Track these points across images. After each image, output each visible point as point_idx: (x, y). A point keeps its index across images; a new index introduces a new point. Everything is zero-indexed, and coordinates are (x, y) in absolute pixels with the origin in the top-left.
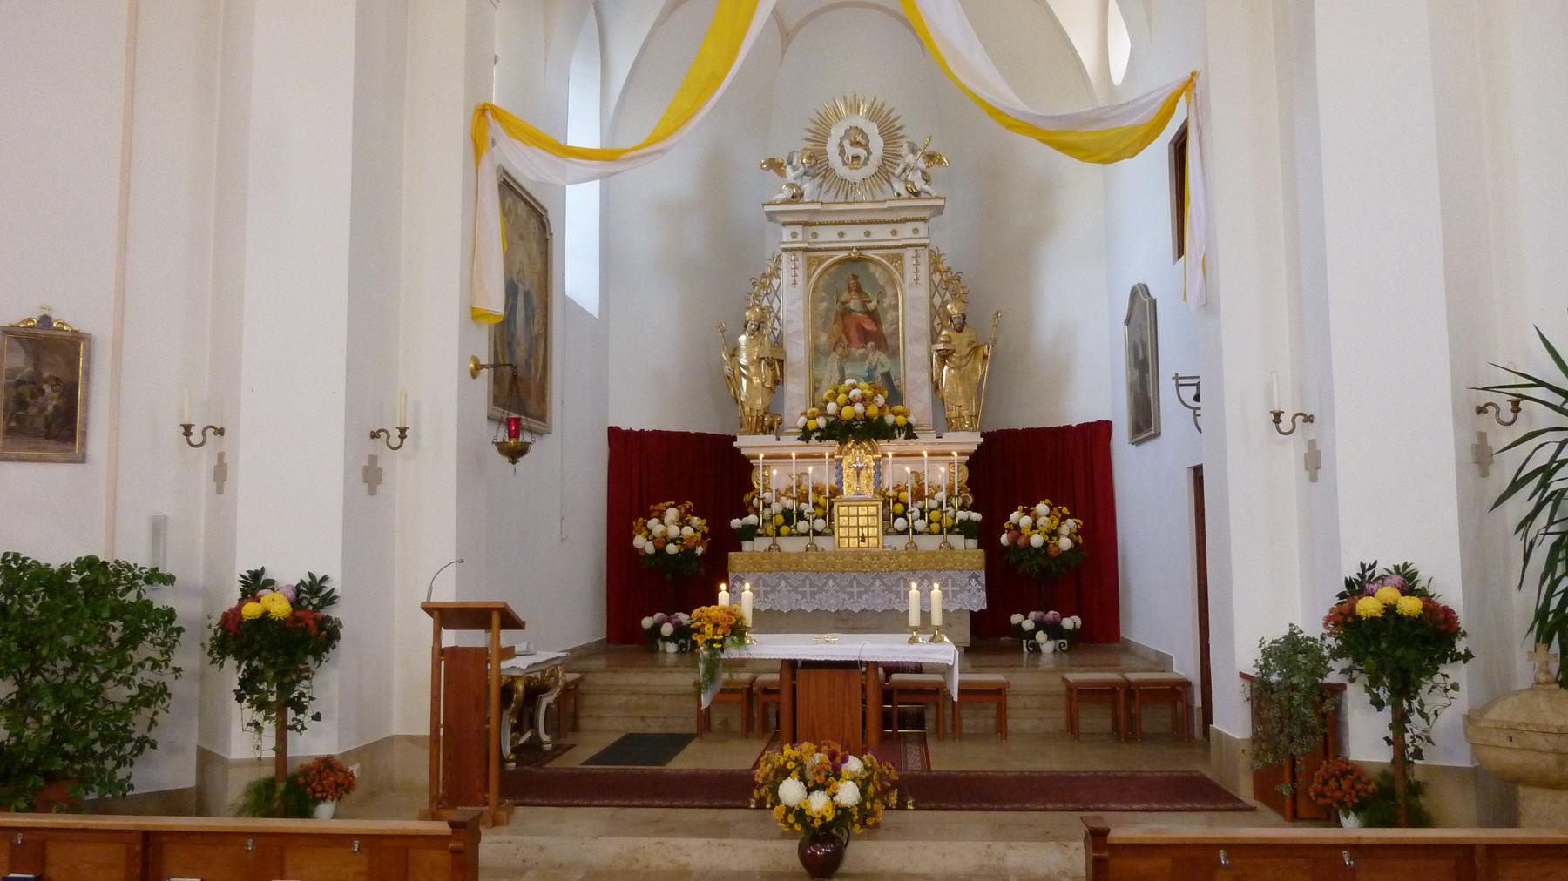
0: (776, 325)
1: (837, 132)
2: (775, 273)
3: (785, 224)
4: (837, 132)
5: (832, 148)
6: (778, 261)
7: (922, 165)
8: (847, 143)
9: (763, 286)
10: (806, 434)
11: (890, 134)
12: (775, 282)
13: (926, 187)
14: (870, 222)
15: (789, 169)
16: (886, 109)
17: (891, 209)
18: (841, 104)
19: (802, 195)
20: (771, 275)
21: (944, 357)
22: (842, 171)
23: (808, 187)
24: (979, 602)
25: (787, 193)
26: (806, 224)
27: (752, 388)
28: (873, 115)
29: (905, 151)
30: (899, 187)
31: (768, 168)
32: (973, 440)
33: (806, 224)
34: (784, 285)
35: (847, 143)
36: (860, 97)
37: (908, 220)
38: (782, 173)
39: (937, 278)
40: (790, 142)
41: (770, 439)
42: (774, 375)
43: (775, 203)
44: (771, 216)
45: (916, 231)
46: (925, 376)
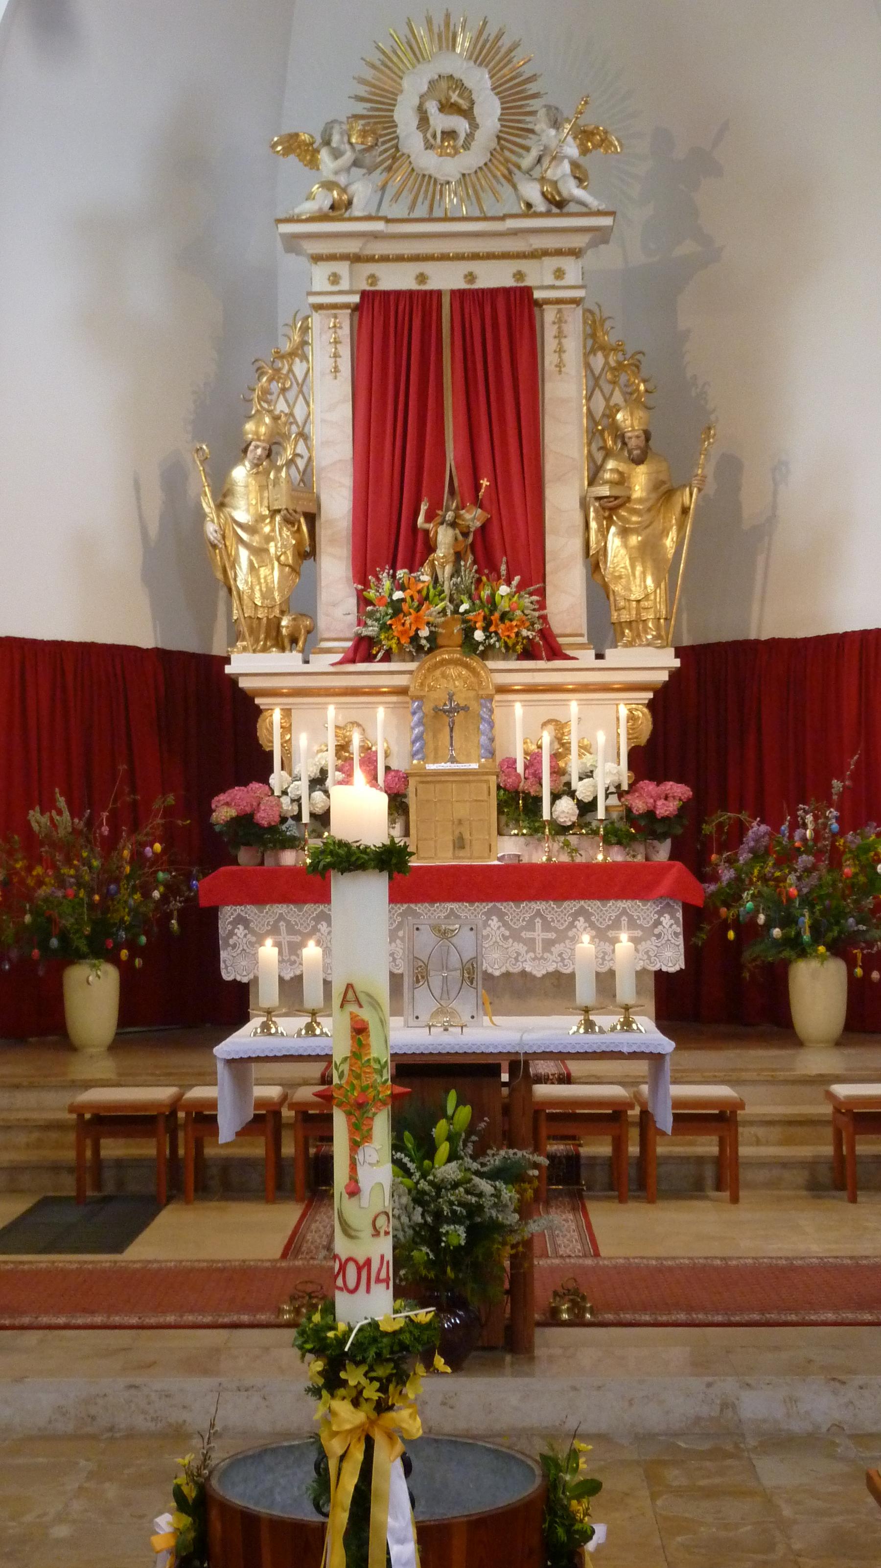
0: (301, 448)
1: (413, 86)
2: (300, 351)
3: (317, 258)
4: (413, 86)
5: (405, 117)
6: (305, 329)
7: (572, 150)
8: (432, 107)
9: (276, 376)
10: (364, 649)
11: (515, 96)
12: (299, 368)
13: (579, 193)
14: (476, 257)
15: (324, 155)
16: (506, 42)
17: (515, 233)
18: (421, 32)
19: (350, 203)
20: (292, 354)
21: (612, 508)
22: (429, 162)
23: (362, 192)
24: (673, 959)
25: (322, 201)
26: (356, 259)
27: (256, 578)
28: (485, 53)
29: (541, 124)
30: (532, 191)
31: (287, 151)
32: (659, 663)
33: (356, 259)
34: (316, 376)
35: (432, 107)
36: (457, 19)
37: (546, 253)
38: (313, 164)
39: (598, 361)
40: (323, 99)
41: (291, 660)
42: (300, 543)
43: (299, 221)
44: (292, 243)
45: (559, 273)
46: (576, 545)
